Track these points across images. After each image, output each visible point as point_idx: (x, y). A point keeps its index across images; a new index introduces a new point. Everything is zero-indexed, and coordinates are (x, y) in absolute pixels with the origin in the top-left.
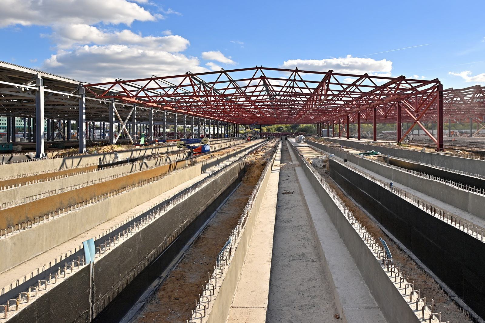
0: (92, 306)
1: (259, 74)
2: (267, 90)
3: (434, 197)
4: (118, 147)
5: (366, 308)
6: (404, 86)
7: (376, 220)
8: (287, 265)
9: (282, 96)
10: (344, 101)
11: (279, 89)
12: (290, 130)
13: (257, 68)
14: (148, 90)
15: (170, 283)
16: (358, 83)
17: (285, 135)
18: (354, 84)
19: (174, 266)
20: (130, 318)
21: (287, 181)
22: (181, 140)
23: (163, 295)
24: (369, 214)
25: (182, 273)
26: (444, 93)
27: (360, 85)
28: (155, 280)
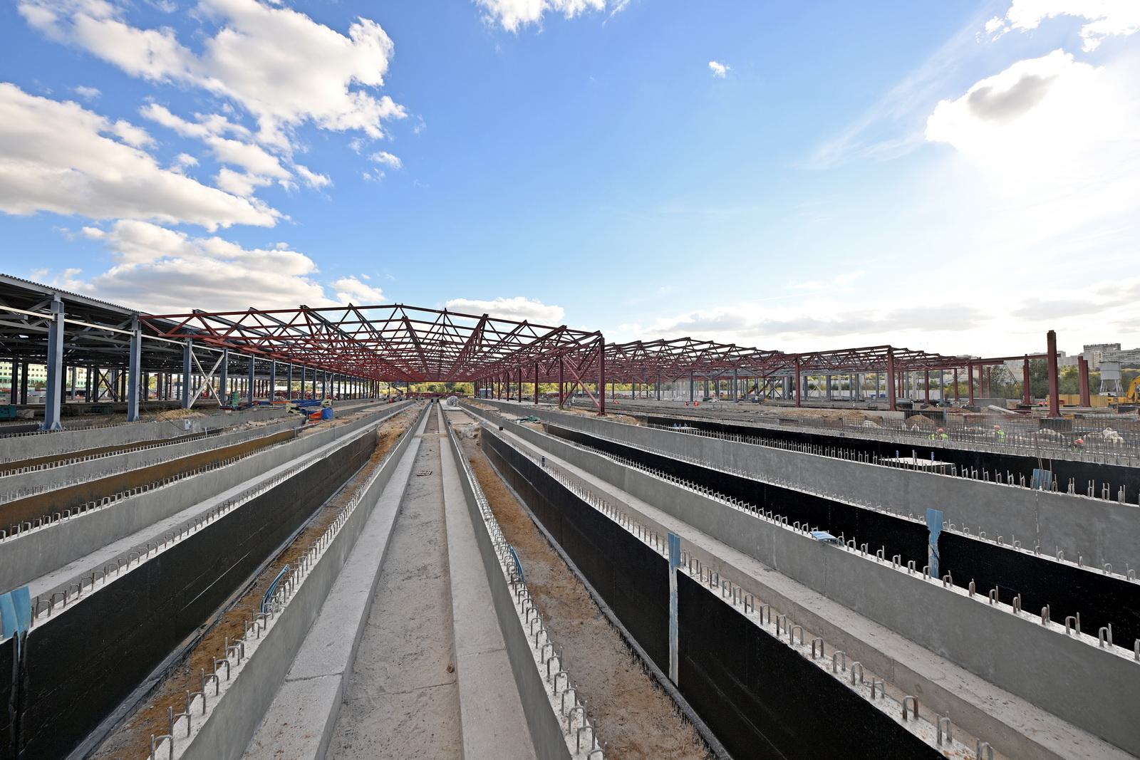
0: (18, 716)
1: (399, 315)
2: (412, 336)
3: (591, 473)
4: (194, 412)
5: (488, 652)
6: (566, 337)
7: (527, 507)
8: (399, 588)
9: (428, 344)
10: (502, 354)
11: (423, 335)
12: (443, 390)
13: (396, 306)
14: (246, 329)
15: (218, 634)
16: (516, 333)
17: (438, 396)
18: (512, 333)
19: (233, 603)
20: (121, 716)
21: (427, 458)
22: (293, 402)
23: (200, 659)
24: (520, 498)
25: (245, 612)
26: (606, 348)
27: (518, 335)
28: (192, 632)
